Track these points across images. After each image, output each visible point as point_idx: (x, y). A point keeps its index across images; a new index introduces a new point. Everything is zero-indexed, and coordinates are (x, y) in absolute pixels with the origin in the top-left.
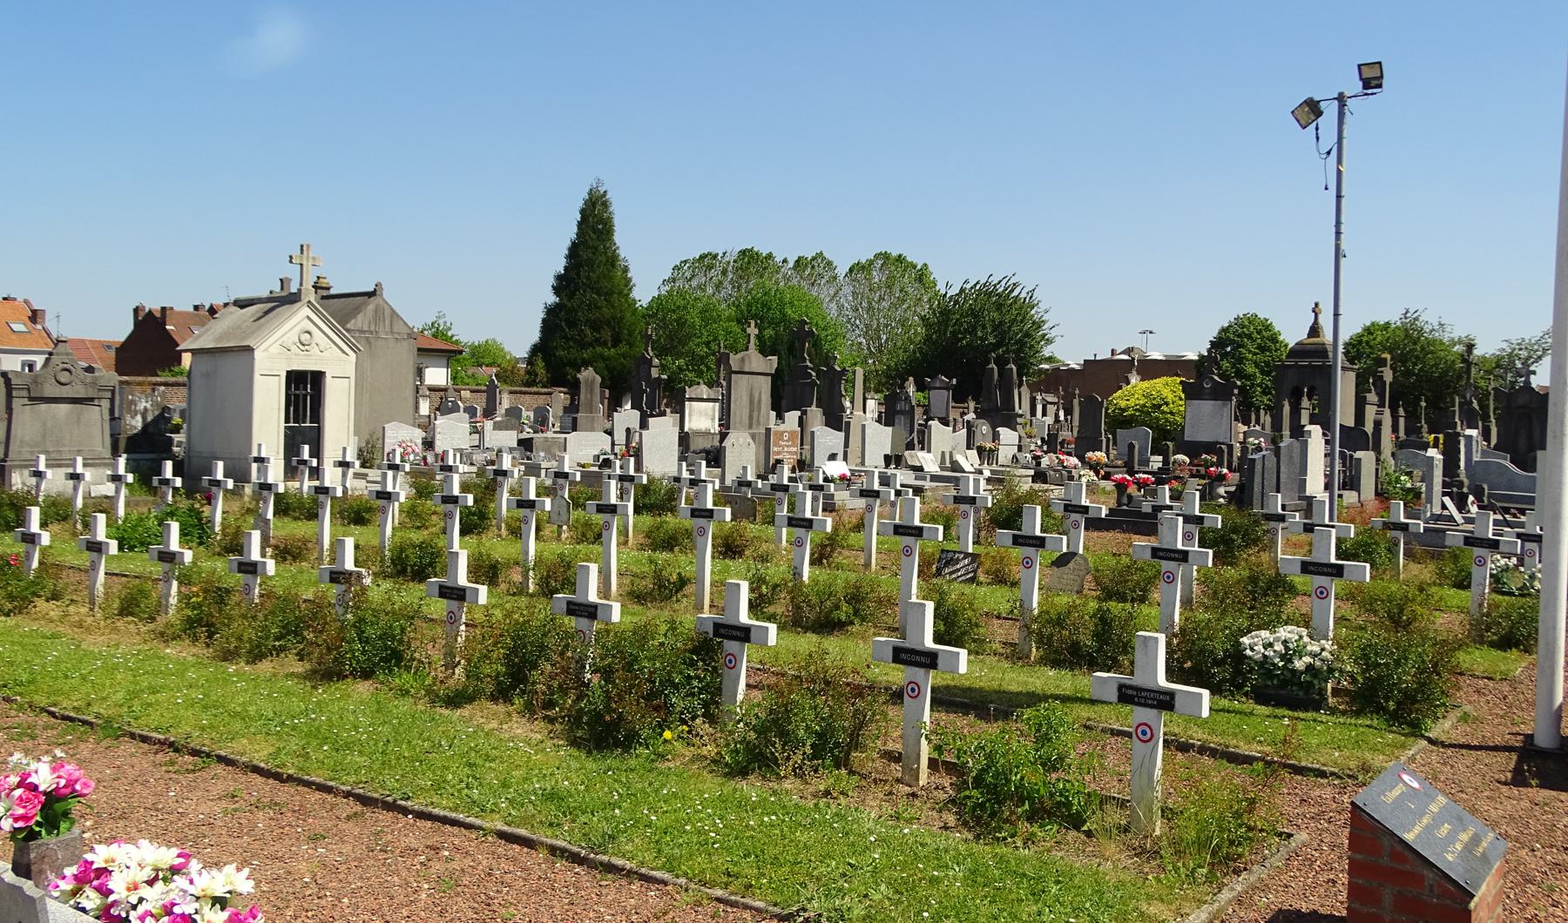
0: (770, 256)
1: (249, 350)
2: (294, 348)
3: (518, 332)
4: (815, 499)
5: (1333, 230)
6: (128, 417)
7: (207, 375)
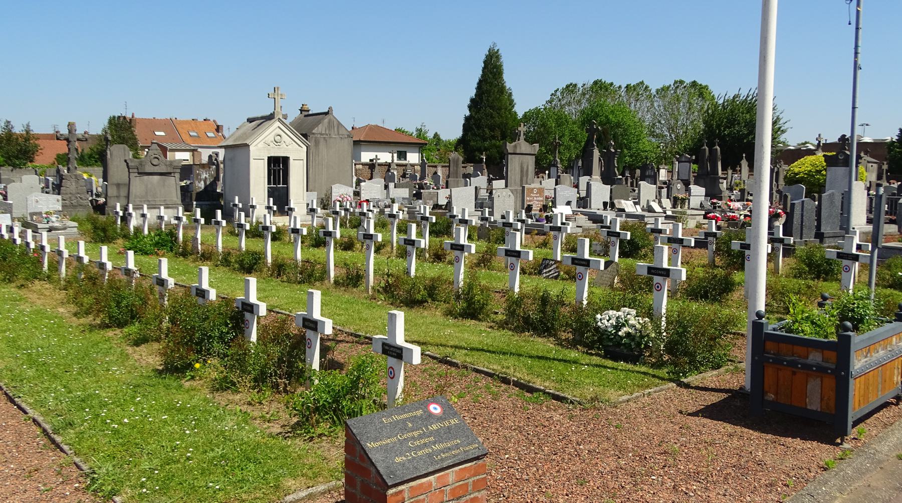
0: (612, 84)
1: (247, 146)
2: (272, 144)
3: (453, 132)
4: (335, 220)
5: (853, 51)
6: (197, 182)
7: (231, 160)
